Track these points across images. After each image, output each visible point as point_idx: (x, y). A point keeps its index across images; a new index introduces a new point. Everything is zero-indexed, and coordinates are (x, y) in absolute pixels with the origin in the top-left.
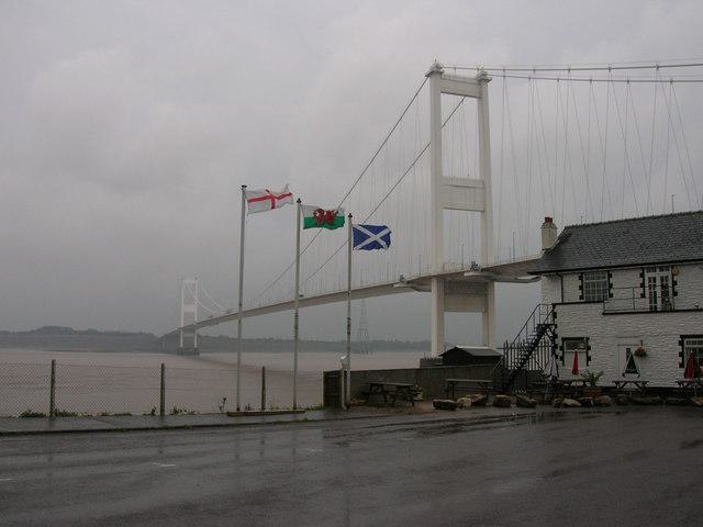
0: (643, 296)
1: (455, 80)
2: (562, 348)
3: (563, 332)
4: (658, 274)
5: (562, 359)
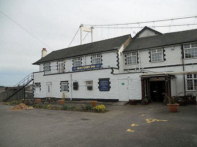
4: (61, 63)
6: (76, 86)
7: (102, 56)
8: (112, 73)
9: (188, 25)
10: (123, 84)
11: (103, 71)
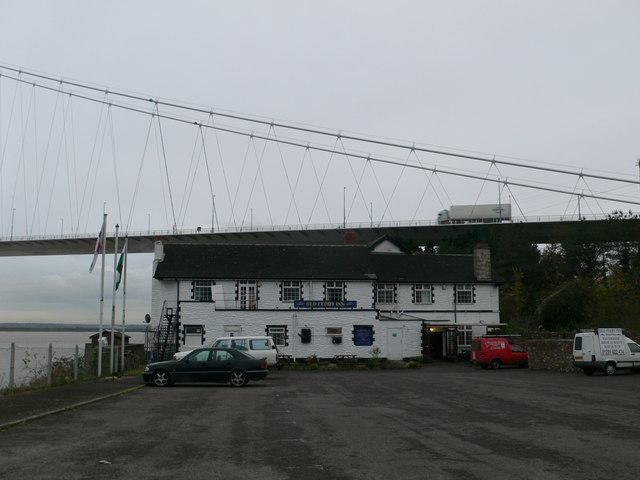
0: (237, 299)
2: (183, 332)
4: (248, 286)
5: (183, 340)
6: (306, 336)
7: (345, 286)
9: (308, 147)
10: (395, 335)
11: (257, 313)
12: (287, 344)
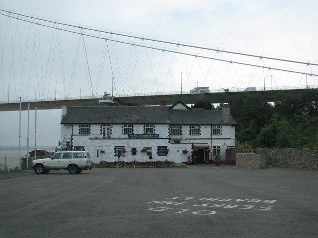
0: (101, 133)
1: (96, 165)
3: (75, 144)
4: (106, 127)
8: (169, 142)
10: (178, 151)
12: (124, 156)
